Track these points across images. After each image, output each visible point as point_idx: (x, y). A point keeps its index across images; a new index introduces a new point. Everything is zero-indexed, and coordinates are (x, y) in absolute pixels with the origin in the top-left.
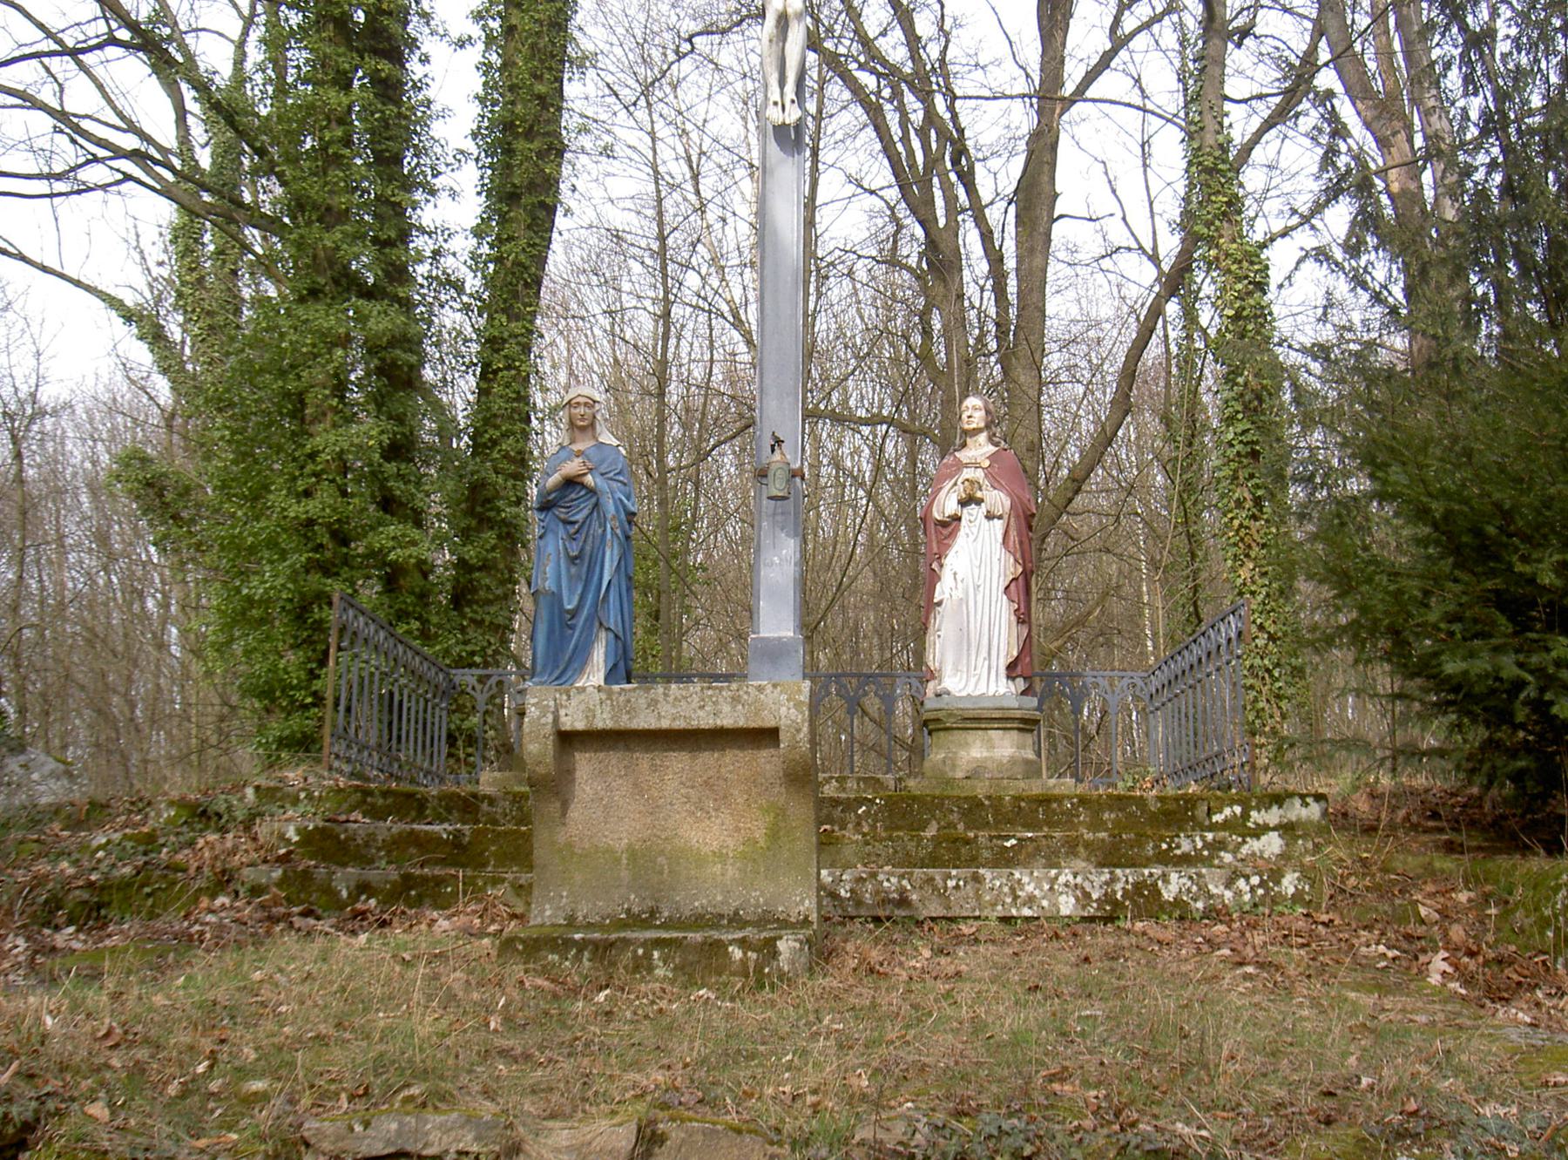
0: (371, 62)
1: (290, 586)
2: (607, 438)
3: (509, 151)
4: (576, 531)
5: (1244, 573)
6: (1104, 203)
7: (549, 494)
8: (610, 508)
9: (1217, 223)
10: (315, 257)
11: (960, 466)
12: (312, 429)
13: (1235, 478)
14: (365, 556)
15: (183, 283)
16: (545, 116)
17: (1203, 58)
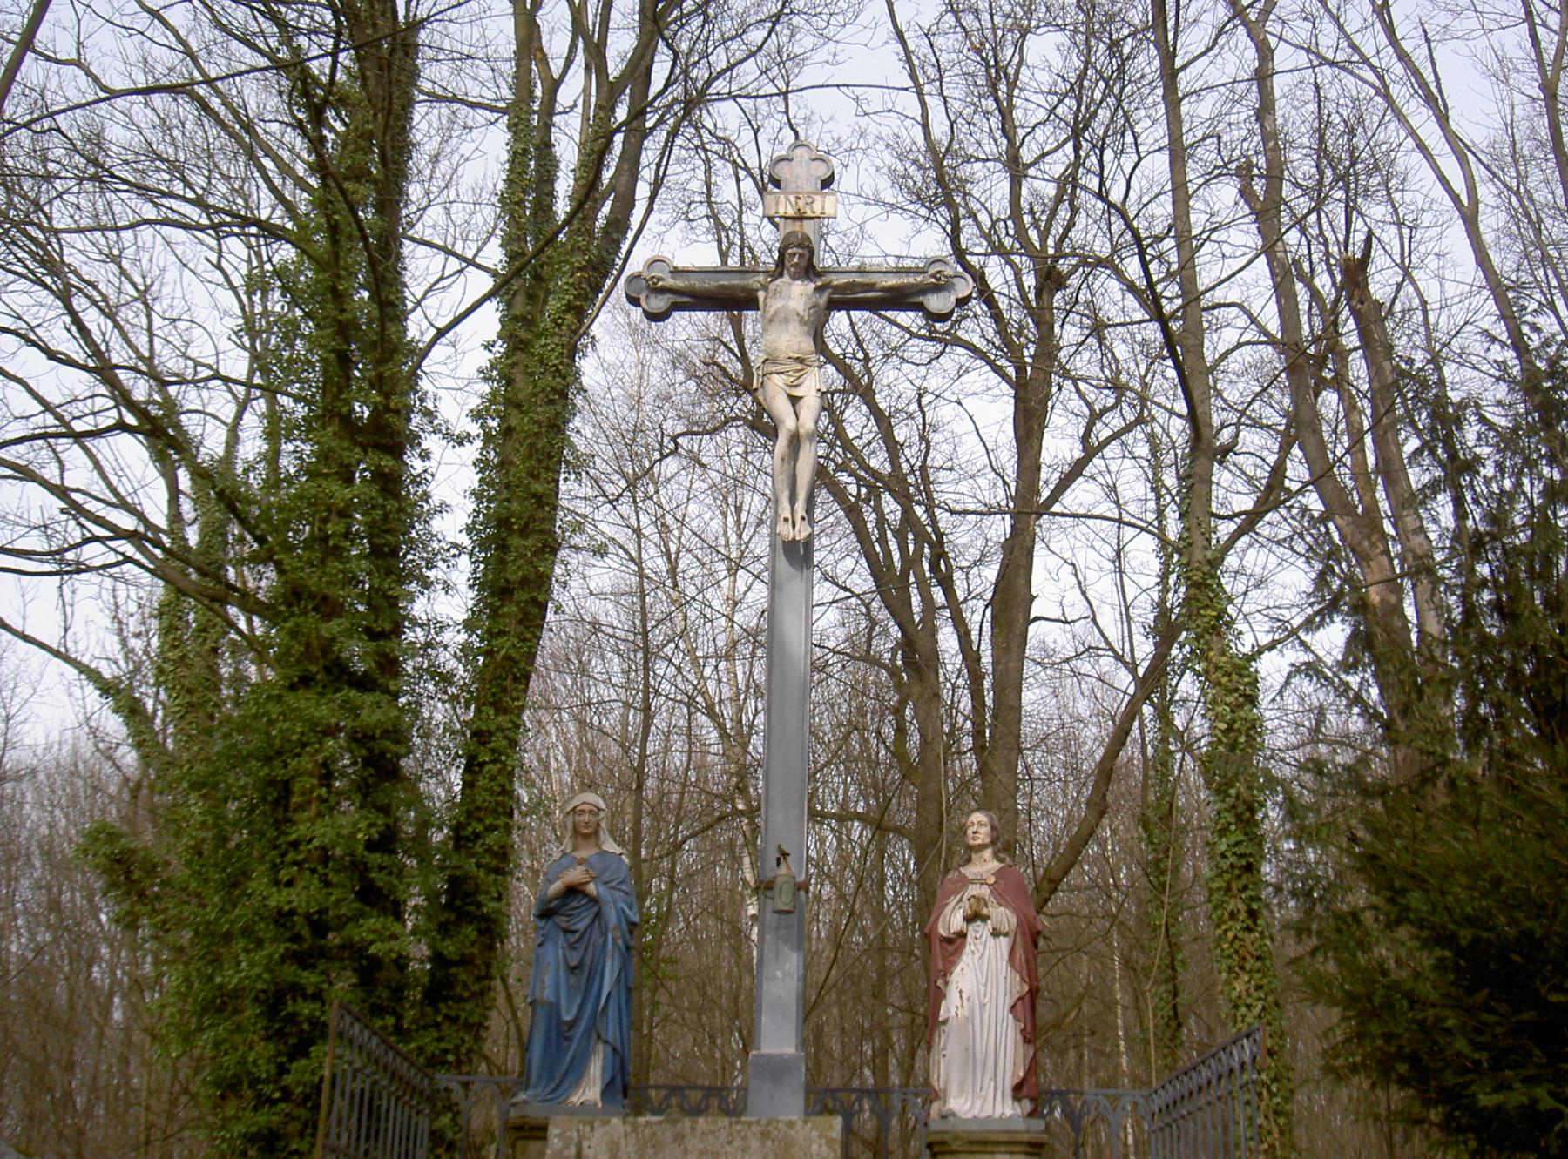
0: (373, 457)
1: (266, 976)
2: (610, 846)
3: (503, 547)
4: (576, 939)
5: (1239, 986)
6: (1076, 608)
7: (551, 901)
8: (612, 917)
9: (1207, 636)
10: (308, 645)
11: (965, 882)
12: (296, 817)
13: (1228, 889)
14: (342, 947)
15: (165, 660)
16: (540, 514)
17: (1190, 476)
